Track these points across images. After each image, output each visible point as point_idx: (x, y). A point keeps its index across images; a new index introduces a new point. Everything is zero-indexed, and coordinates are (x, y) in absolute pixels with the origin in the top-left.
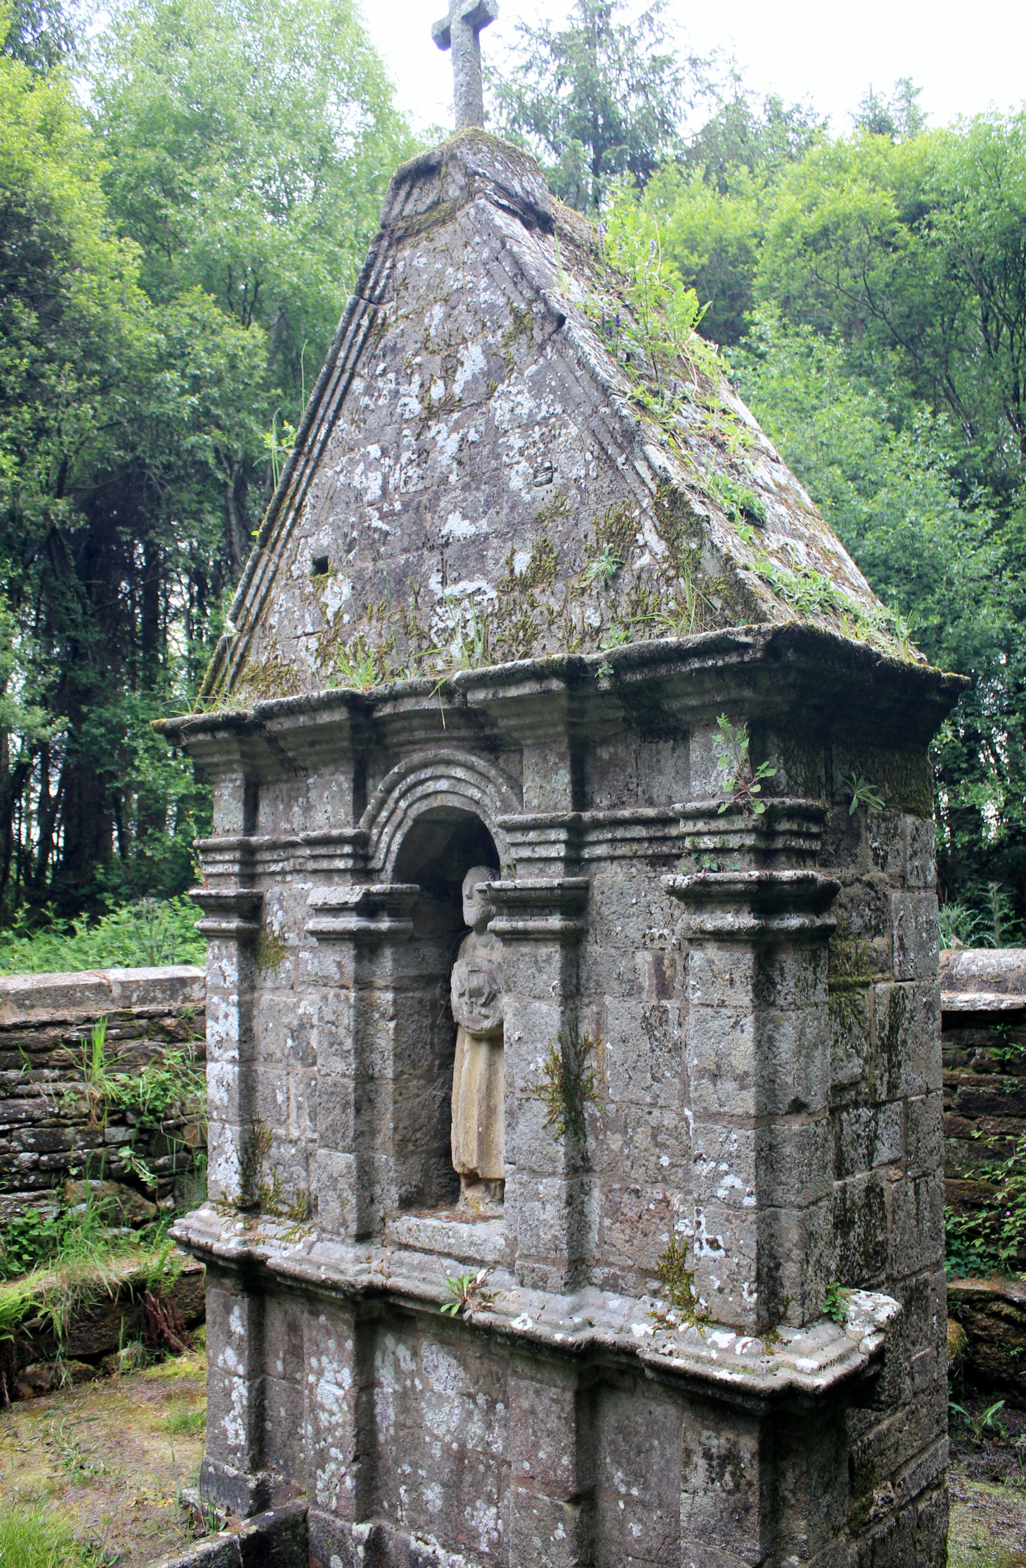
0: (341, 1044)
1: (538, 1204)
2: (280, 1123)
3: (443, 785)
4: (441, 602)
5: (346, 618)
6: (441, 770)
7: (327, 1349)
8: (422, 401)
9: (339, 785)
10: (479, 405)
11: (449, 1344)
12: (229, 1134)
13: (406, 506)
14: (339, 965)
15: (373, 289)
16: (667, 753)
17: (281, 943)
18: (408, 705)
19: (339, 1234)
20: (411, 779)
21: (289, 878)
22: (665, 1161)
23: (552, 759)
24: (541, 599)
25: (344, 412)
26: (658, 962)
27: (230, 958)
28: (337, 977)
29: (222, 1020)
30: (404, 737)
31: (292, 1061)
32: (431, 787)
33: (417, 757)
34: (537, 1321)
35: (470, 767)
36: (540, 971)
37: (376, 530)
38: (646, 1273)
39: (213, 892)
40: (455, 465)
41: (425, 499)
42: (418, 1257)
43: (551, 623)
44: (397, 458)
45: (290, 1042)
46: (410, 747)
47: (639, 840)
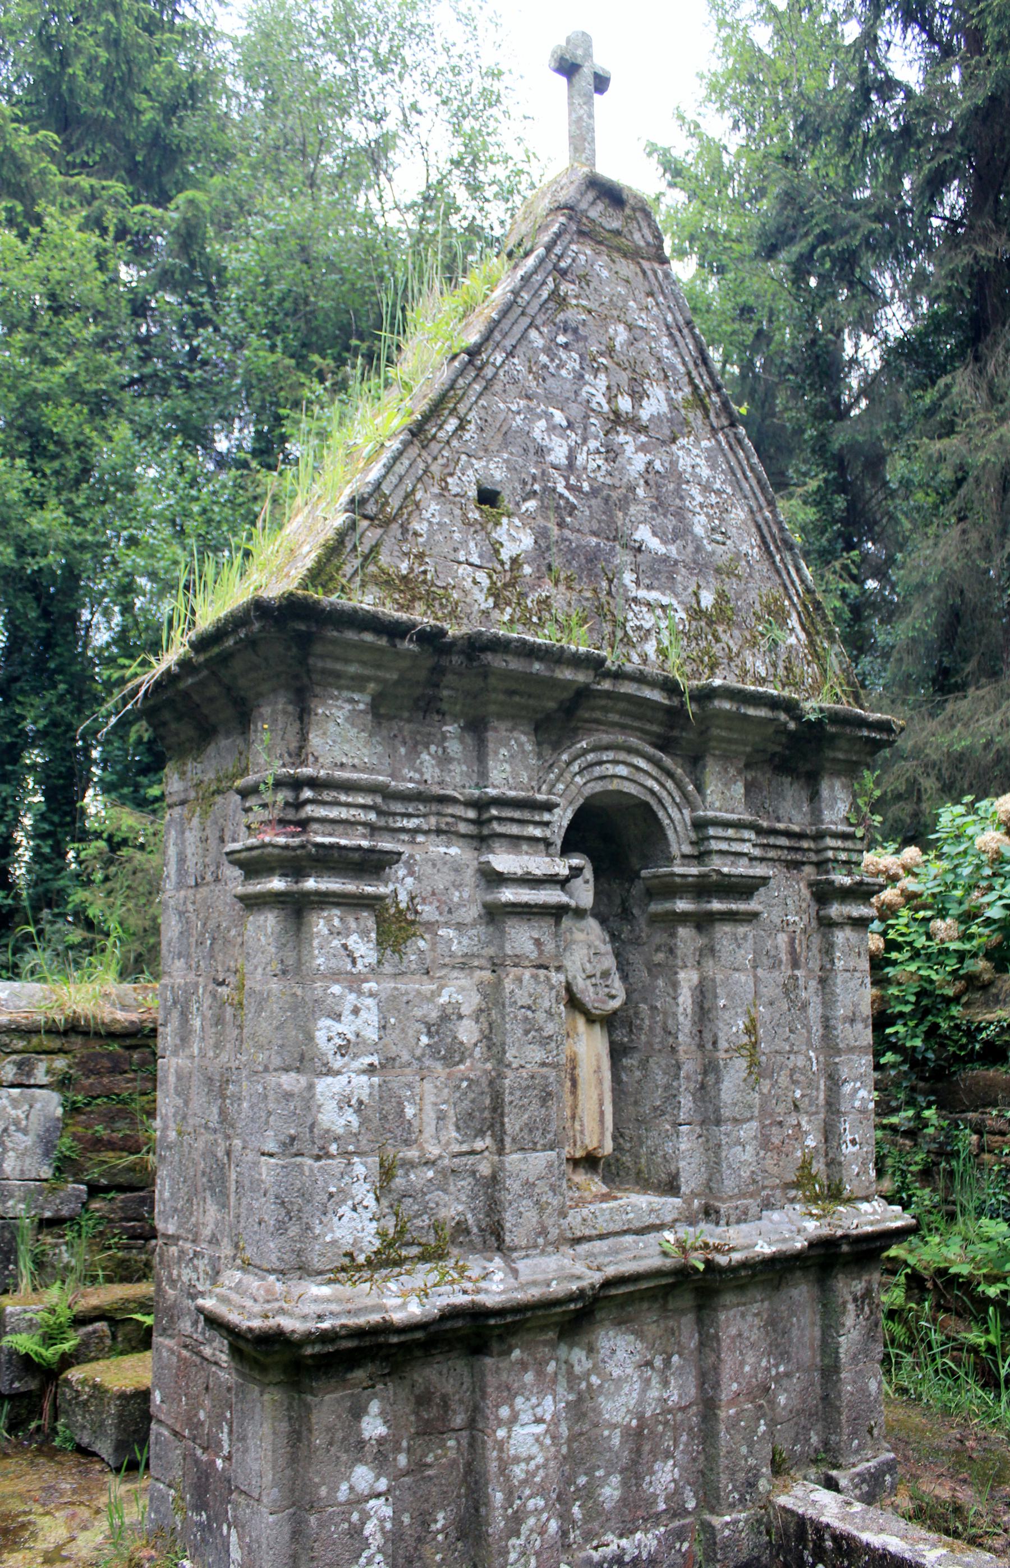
0: (540, 1029)
1: (740, 1148)
2: (407, 1143)
3: (622, 770)
4: (635, 600)
5: (527, 570)
6: (622, 756)
7: (524, 1386)
8: (609, 402)
9: (521, 745)
10: (664, 442)
11: (625, 1322)
12: (359, 1169)
13: (595, 492)
14: (538, 943)
15: (560, 257)
16: (787, 786)
17: (410, 917)
18: (628, 688)
19: (535, 1246)
20: (591, 757)
21: (420, 838)
22: (798, 1094)
23: (732, 771)
24: (725, 637)
25: (519, 350)
26: (792, 942)
27: (364, 933)
28: (534, 956)
29: (347, 1017)
30: (598, 715)
31: (428, 1062)
32: (610, 769)
33: (606, 738)
34: (770, 1244)
35: (649, 759)
36: (739, 946)
37: (561, 496)
38: (788, 1186)
39: (365, 843)
40: (642, 482)
41: (614, 495)
42: (611, 1241)
43: (731, 659)
44: (585, 440)
45: (424, 1040)
46: (594, 726)
47: (781, 847)
